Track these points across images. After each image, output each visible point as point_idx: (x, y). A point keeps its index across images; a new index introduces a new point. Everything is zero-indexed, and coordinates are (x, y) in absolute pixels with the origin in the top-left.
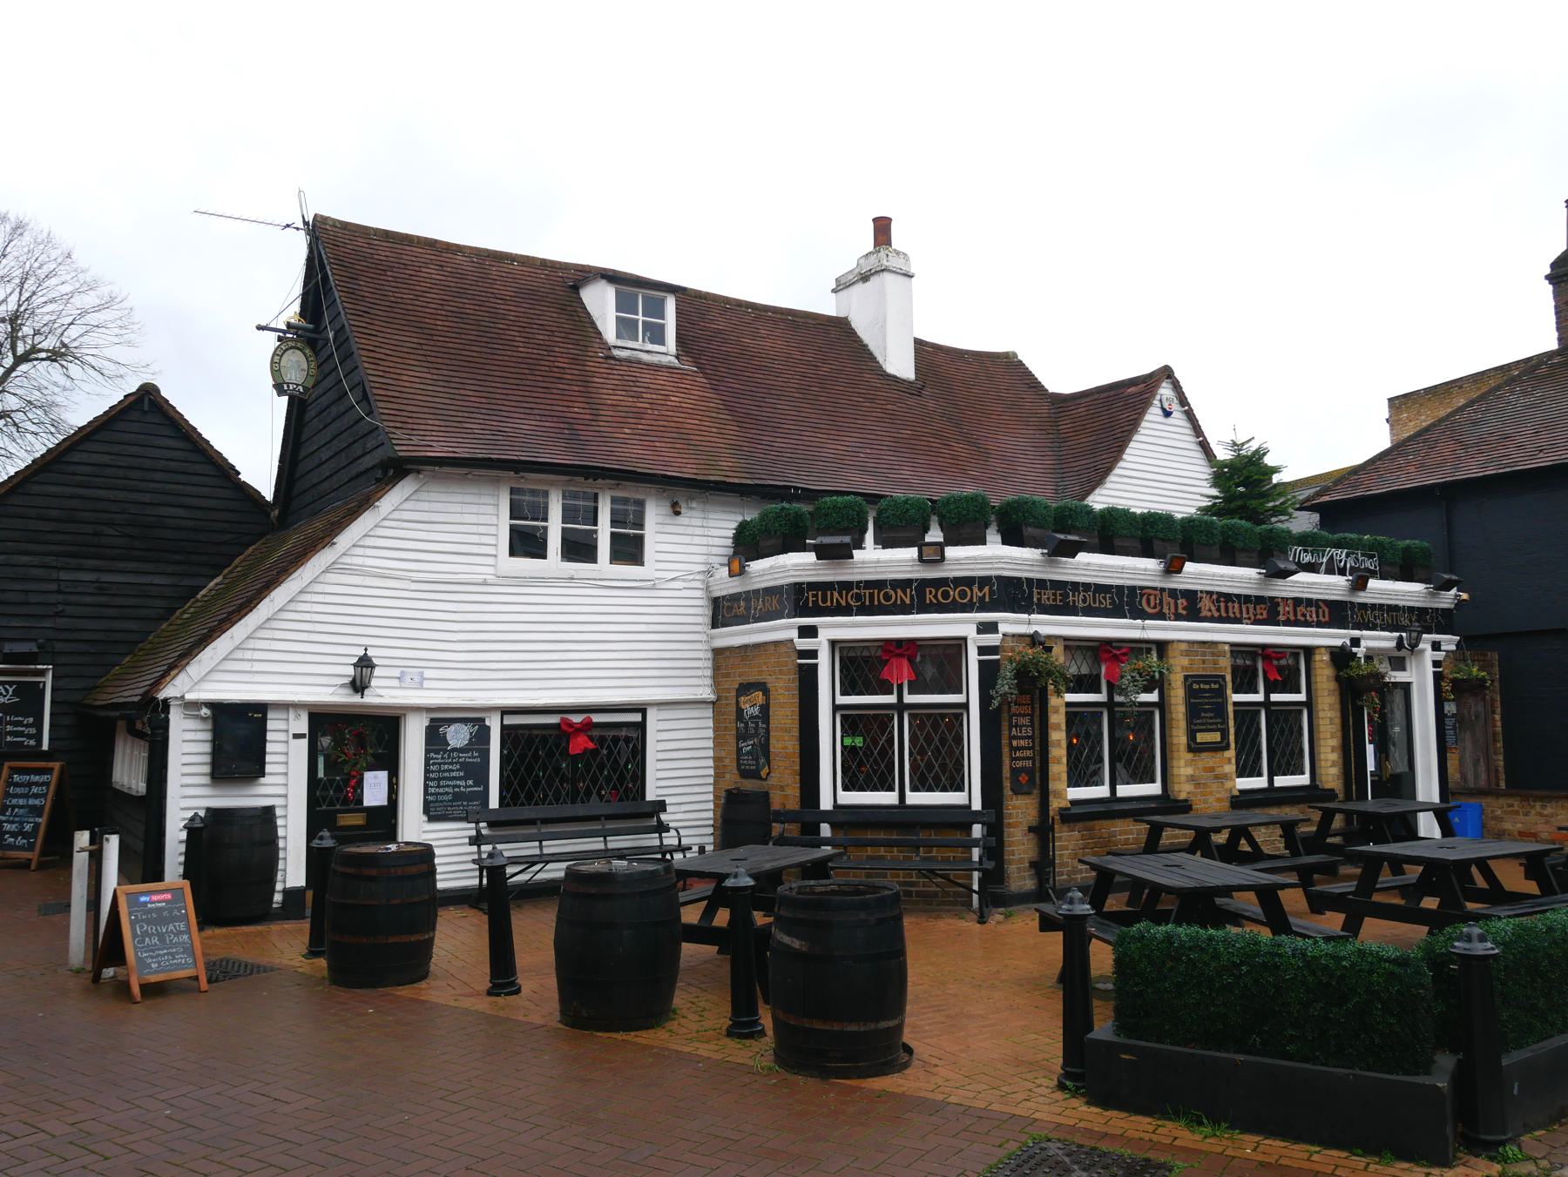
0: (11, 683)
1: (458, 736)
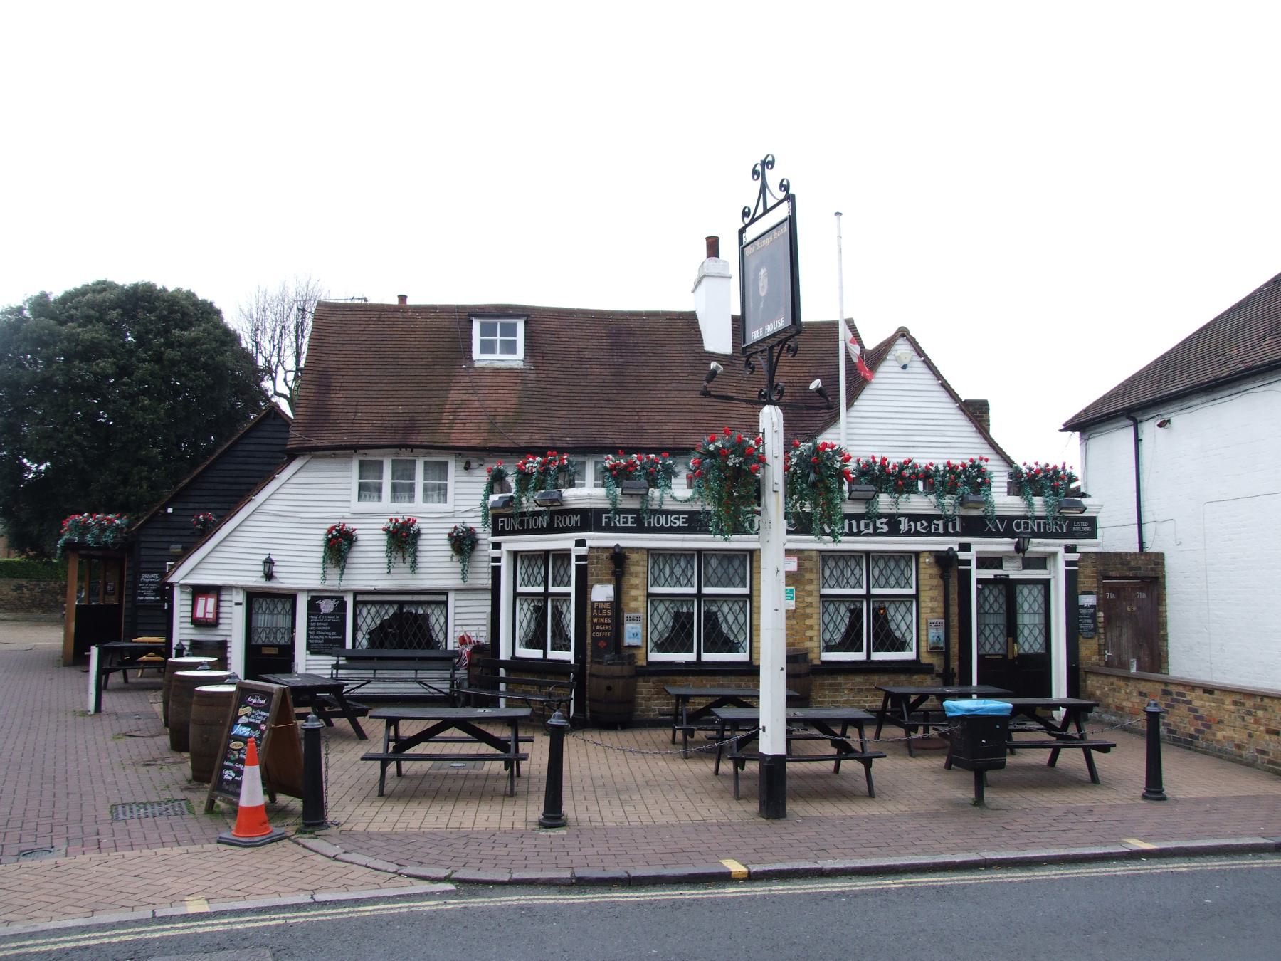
1: (327, 607)
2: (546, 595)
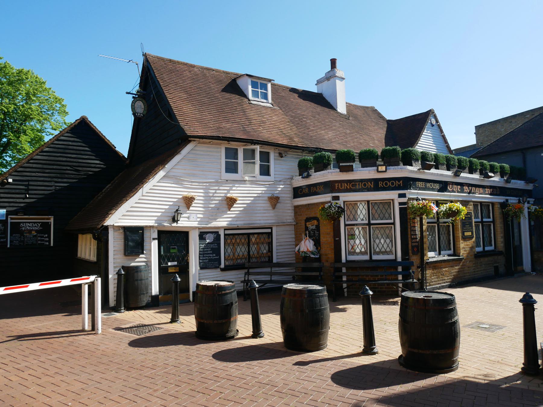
0: (39, 223)
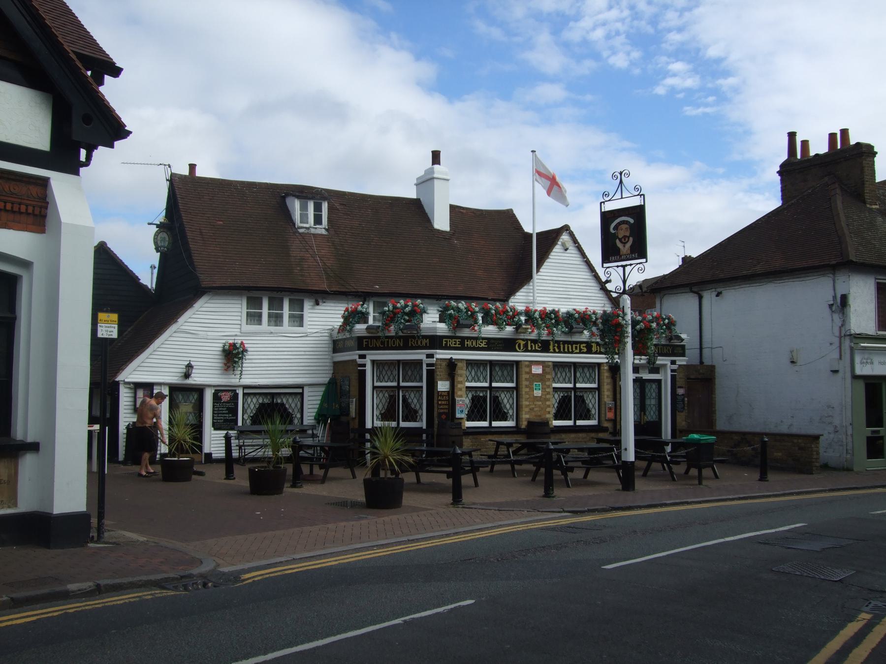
1: (226, 397)
2: (399, 387)
